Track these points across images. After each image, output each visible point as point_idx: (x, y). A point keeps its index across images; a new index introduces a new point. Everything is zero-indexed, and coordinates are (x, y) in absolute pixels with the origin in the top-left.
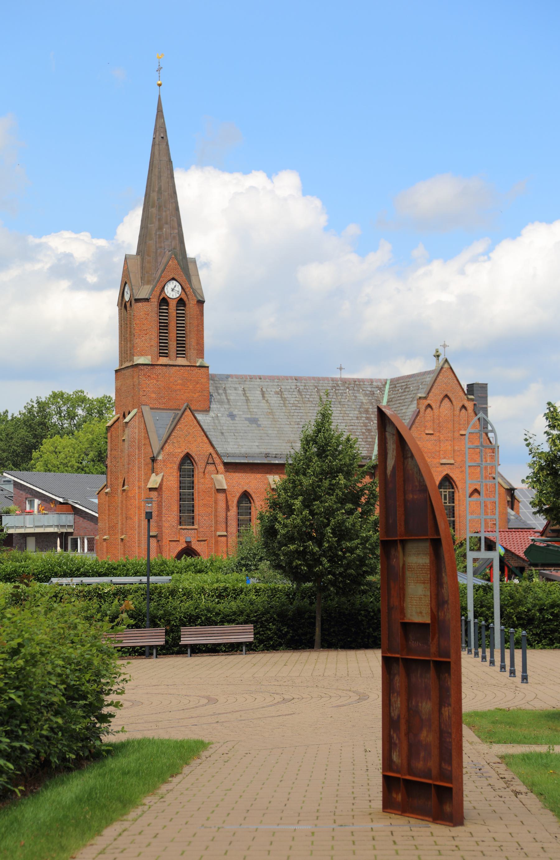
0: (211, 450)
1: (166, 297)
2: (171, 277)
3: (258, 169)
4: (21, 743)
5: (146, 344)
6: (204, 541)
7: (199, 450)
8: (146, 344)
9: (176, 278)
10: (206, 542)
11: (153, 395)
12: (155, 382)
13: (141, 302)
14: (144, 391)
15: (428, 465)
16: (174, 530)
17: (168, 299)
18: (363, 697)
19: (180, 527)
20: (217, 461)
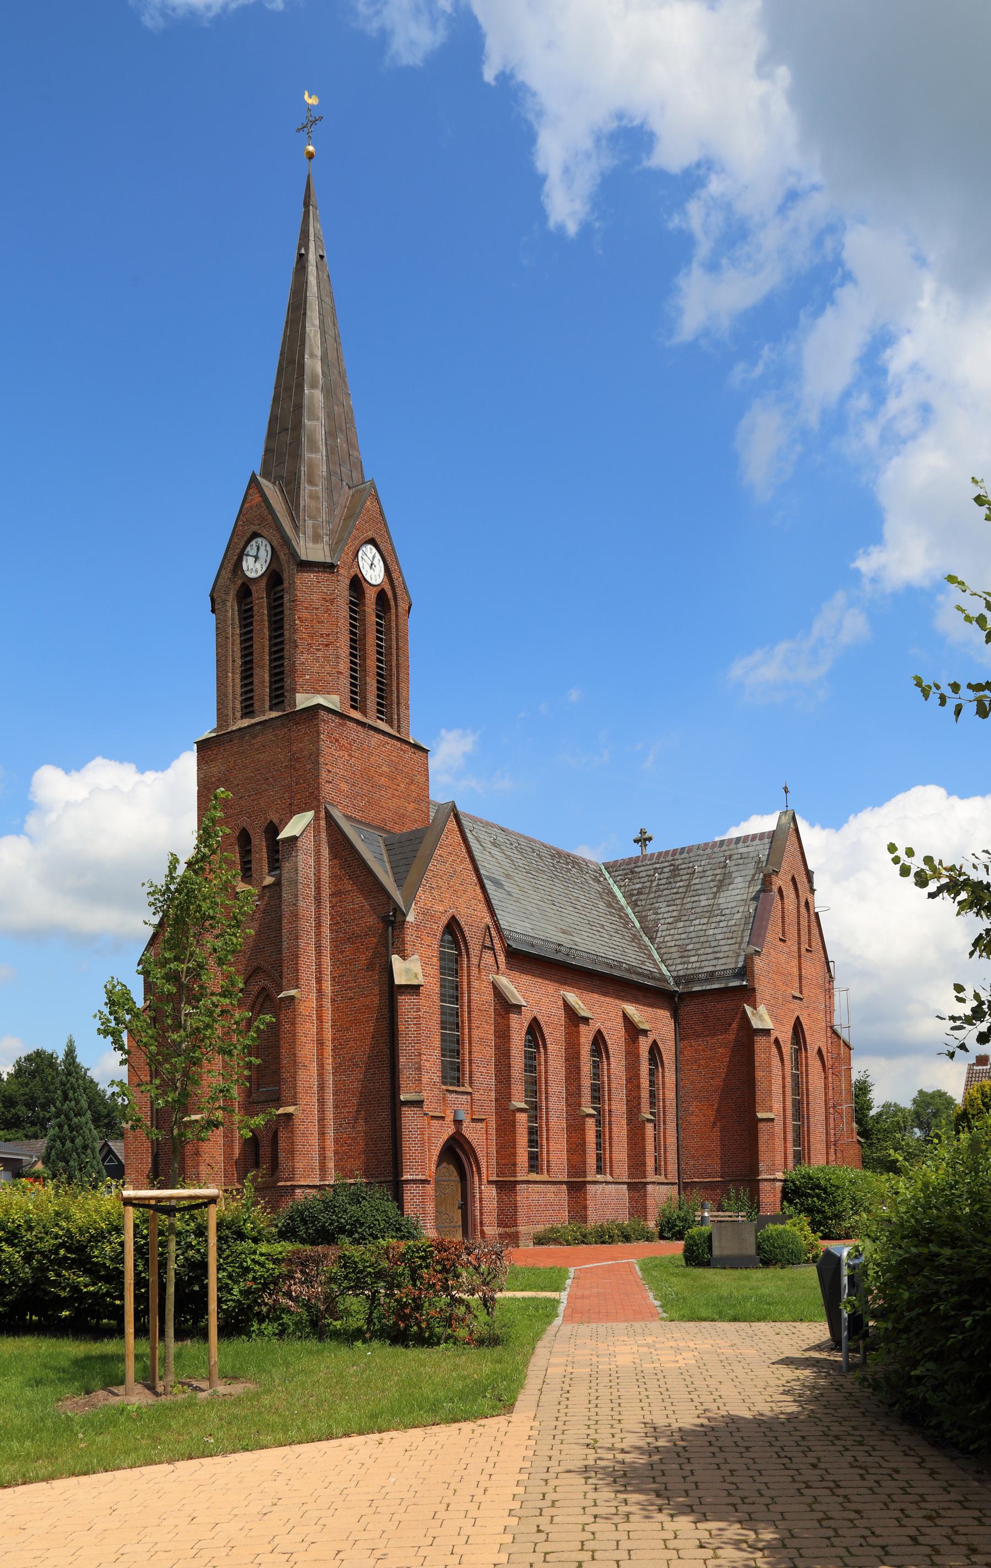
0: (488, 920)
1: (360, 576)
2: (370, 534)
3: (925, 781)
4: (562, 1315)
5: (328, 668)
6: (481, 1120)
7: (474, 919)
8: (328, 668)
9: (378, 540)
10: (482, 1125)
11: (344, 786)
12: (347, 757)
13: (313, 572)
14: (329, 771)
15: (277, 1163)
16: (436, 1092)
17: (365, 584)
18: (815, 1289)
19: (444, 1087)
20: (498, 946)
